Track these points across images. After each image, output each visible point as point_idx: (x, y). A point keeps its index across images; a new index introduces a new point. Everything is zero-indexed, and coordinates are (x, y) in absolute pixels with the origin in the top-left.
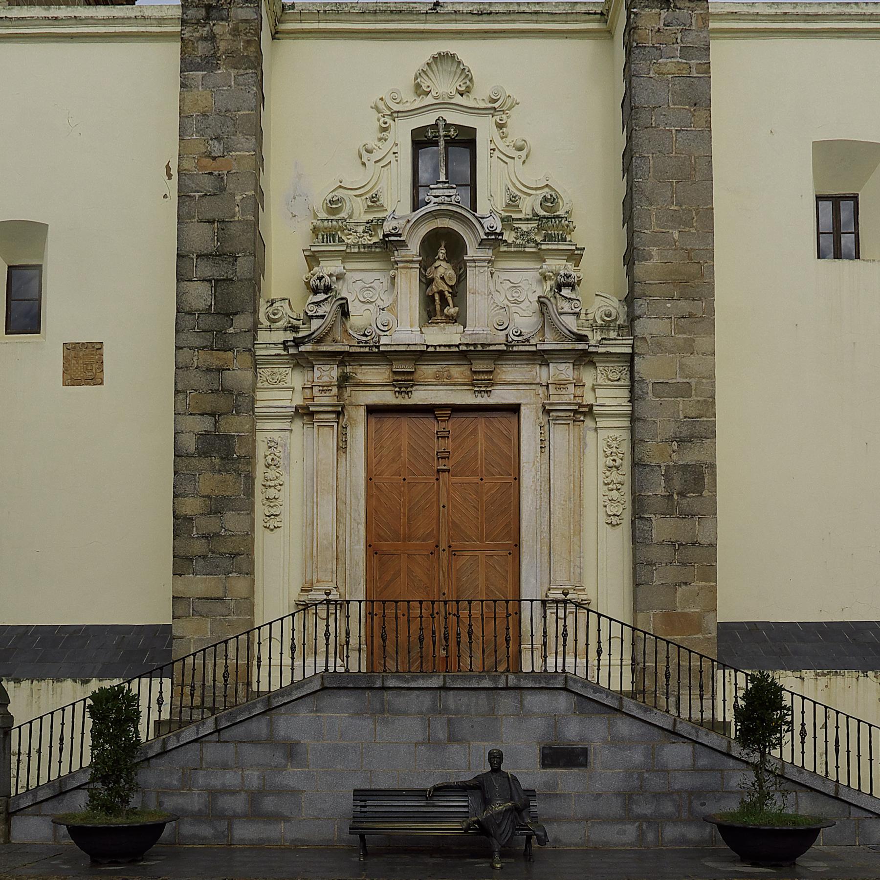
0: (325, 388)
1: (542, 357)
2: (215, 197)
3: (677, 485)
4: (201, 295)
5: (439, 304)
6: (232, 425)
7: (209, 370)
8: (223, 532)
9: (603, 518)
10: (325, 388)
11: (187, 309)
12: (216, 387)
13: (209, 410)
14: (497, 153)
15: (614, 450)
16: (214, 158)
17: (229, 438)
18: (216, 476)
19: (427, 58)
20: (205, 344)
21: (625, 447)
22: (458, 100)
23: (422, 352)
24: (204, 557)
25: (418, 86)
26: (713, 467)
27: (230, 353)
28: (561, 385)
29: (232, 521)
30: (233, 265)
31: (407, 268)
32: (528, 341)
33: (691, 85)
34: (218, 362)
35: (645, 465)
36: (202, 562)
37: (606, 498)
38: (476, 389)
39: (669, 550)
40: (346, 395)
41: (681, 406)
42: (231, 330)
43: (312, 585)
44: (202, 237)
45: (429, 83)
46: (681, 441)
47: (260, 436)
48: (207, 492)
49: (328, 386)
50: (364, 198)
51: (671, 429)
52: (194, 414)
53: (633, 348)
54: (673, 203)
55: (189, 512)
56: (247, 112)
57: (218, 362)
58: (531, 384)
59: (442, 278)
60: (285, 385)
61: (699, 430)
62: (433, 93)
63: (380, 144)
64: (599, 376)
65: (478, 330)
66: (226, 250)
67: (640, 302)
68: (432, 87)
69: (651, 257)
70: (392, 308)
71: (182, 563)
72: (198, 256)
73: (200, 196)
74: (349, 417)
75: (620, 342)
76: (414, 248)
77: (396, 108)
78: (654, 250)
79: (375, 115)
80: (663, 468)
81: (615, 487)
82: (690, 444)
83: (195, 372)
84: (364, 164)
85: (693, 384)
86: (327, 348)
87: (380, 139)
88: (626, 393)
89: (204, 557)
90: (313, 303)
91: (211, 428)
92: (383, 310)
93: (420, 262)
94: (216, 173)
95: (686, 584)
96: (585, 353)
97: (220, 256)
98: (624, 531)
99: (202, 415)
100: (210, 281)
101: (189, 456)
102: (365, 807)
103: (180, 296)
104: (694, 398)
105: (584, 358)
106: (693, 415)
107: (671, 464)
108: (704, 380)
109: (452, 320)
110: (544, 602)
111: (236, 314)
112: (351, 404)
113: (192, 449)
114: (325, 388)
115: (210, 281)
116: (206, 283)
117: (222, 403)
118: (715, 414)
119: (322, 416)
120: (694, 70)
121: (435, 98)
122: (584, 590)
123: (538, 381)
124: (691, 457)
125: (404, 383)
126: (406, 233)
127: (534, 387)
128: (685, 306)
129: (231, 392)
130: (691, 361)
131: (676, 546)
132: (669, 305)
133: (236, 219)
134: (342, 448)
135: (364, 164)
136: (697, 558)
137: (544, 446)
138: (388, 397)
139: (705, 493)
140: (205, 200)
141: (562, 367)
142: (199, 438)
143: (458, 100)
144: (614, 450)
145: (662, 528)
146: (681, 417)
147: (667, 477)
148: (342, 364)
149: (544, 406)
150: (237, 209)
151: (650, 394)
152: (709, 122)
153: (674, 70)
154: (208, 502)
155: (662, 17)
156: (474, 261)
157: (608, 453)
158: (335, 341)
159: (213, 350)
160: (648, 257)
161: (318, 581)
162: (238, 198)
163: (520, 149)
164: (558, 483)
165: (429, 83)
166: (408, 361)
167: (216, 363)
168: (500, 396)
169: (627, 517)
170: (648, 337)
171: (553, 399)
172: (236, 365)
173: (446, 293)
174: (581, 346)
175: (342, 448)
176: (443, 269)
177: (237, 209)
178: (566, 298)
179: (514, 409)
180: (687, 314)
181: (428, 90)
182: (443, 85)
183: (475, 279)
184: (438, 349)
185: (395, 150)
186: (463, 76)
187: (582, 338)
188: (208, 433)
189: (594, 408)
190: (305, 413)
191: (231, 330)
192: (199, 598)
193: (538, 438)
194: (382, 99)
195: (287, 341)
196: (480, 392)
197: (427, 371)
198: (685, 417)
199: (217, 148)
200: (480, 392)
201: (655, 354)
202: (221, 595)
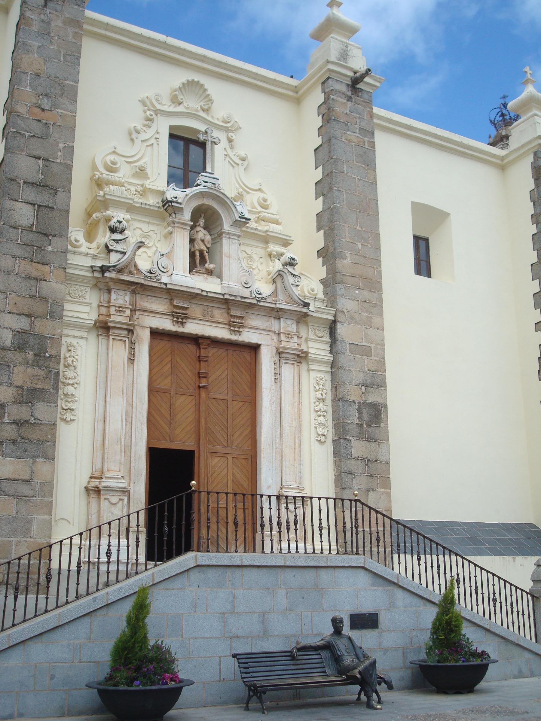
0: (121, 309)
1: (277, 313)
2: (42, 140)
5: (198, 261)
6: (43, 327)
7: (28, 278)
8: (32, 420)
9: (314, 436)
10: (120, 309)
11: (12, 223)
12: (33, 293)
13: (26, 311)
15: (321, 387)
16: (43, 110)
17: (42, 337)
18: (30, 370)
19: (184, 80)
20: (26, 256)
21: (328, 386)
22: (202, 114)
23: (197, 294)
24: (14, 442)
25: (176, 97)
26: (386, 406)
27: (47, 267)
28: (289, 335)
29: (41, 411)
30: (54, 196)
31: (182, 228)
32: (265, 299)
33: (365, 153)
34: (36, 273)
35: (347, 401)
36: (11, 446)
37: (316, 421)
38: (232, 328)
39: (361, 464)
40: (135, 317)
41: (366, 362)
42: (50, 248)
43: (102, 473)
45: (182, 97)
47: (64, 339)
48: (20, 383)
49: (123, 308)
50: (133, 165)
51: (359, 377)
52: (12, 313)
53: (335, 317)
54: (357, 225)
56: (72, 83)
57: (36, 273)
58: (269, 331)
59: (203, 241)
60: (84, 301)
61: (376, 381)
62: (185, 104)
63: (145, 128)
64: (310, 332)
65: (232, 284)
66: (48, 183)
67: (340, 286)
68: (184, 100)
70: (169, 255)
72: (25, 183)
73: (29, 136)
74: (137, 336)
75: (328, 311)
76: (187, 216)
77: (159, 107)
78: (348, 254)
79: (141, 108)
80: (357, 404)
81: (322, 414)
82: (372, 389)
83: (14, 278)
84: (132, 140)
85: (372, 348)
87: (145, 126)
88: (328, 347)
89: (14, 442)
90: (114, 240)
91: (27, 328)
92: (162, 255)
94: (44, 121)
96: (306, 315)
97: (43, 186)
100: (34, 205)
102: (248, 668)
104: (373, 358)
105: (302, 318)
106: (373, 369)
107: (362, 402)
108: (378, 346)
109: (210, 272)
110: (278, 498)
111: (54, 236)
114: (121, 309)
115: (34, 205)
116: (30, 205)
117: (38, 308)
118: (385, 371)
119: (116, 331)
120: (366, 144)
121: (187, 108)
122: (303, 490)
123: (273, 330)
124: (372, 398)
125: (180, 317)
126: (185, 203)
127: (270, 333)
128: (366, 294)
129: (46, 300)
130: (372, 332)
131: (367, 462)
132: (357, 292)
133: (59, 161)
135: (132, 140)
136: (377, 471)
137: (277, 378)
138: (167, 324)
139: (382, 425)
140: (33, 140)
141: (289, 322)
142: (15, 335)
143: (202, 114)
144: (321, 387)
145: (358, 448)
146: (366, 369)
147: (360, 413)
148: (133, 292)
149: (277, 349)
150: (59, 154)
151: (348, 351)
152: (375, 178)
153: (356, 141)
154: (20, 392)
157: (317, 388)
158: (131, 273)
159: (32, 261)
160: (345, 258)
161: (108, 470)
163: (243, 159)
164: (287, 408)
165: (182, 97)
166: (181, 301)
167: (35, 274)
168: (248, 336)
169: (331, 436)
170: (346, 311)
171: (283, 344)
172: (52, 278)
173: (205, 252)
174: (305, 310)
176: (202, 234)
177: (59, 154)
178: (292, 274)
179: (255, 348)
181: (182, 101)
182: (192, 103)
184: (209, 294)
185: (157, 136)
186: (206, 100)
187: (307, 305)
188: (23, 332)
189: (310, 355)
192: (6, 479)
193: (273, 371)
195: (95, 266)
196: (234, 331)
197: (195, 310)
198: (369, 370)
199: (46, 103)
200: (234, 331)
202: (27, 477)
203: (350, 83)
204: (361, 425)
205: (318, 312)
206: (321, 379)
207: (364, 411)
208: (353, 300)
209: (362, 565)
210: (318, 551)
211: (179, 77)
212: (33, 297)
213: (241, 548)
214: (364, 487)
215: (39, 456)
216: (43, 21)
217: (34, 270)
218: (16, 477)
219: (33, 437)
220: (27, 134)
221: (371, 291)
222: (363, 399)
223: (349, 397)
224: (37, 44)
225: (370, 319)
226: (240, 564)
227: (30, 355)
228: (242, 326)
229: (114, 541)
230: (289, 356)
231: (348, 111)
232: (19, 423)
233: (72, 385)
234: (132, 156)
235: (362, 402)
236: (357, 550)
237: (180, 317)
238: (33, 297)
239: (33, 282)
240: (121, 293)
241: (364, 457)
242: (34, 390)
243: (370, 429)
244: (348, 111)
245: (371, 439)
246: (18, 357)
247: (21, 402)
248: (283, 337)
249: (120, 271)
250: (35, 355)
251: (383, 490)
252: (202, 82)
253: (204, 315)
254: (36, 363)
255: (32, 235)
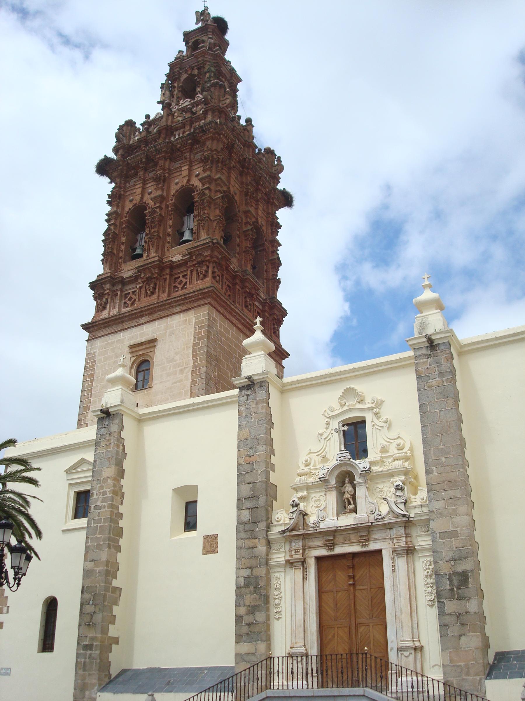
3: (456, 582)
4: (246, 515)
5: (347, 504)
7: (249, 548)
8: (255, 622)
13: (249, 566)
14: (376, 426)
16: (250, 457)
17: (257, 578)
24: (247, 634)
27: (257, 540)
29: (260, 617)
36: (246, 637)
39: (454, 618)
42: (257, 529)
44: (247, 491)
46: (455, 560)
48: (248, 604)
55: (241, 614)
66: (255, 495)
69: (433, 471)
71: (239, 638)
85: (459, 531)
86: (300, 532)
89: (247, 634)
93: (336, 487)
95: (464, 635)
98: (435, 608)
99: (246, 568)
101: (241, 588)
103: (238, 516)
106: (460, 546)
107: (452, 572)
112: (309, 557)
113: (242, 584)
119: (296, 564)
120: (445, 382)
124: (461, 567)
125: (330, 545)
129: (257, 557)
131: (459, 615)
132: (443, 494)
134: (305, 578)
138: (323, 552)
140: (247, 475)
141: (399, 529)
145: (451, 606)
146: (454, 548)
147: (451, 580)
151: (439, 539)
154: (249, 608)
155: (429, 361)
156: (359, 483)
162: (259, 472)
167: (251, 545)
168: (373, 546)
170: (435, 510)
175: (305, 578)
176: (348, 488)
179: (379, 552)
180: (452, 497)
182: (351, 402)
183: (360, 492)
184: (342, 528)
188: (249, 577)
190: (290, 563)
191: (257, 529)
194: (326, 411)
199: (251, 453)
201: (439, 518)
202: (254, 652)
203: (428, 345)
204: (452, 590)
205: (417, 516)
206: (428, 562)
207: (454, 579)
208: (441, 501)
209: (363, 694)
210: (281, 688)
211: (338, 391)
212: (251, 558)
213: (330, 684)
214: (456, 634)
215: (258, 641)
216: (247, 409)
217: (250, 543)
218: (249, 652)
219: (256, 631)
220: (244, 473)
221: (455, 489)
222: (453, 570)
223: (441, 571)
224: (245, 422)
225: (455, 510)
226: (288, 695)
227: (252, 588)
228: (368, 540)
229: (300, 682)
230: (400, 552)
231: (428, 366)
232: (249, 625)
233: (278, 598)
234: (320, 450)
235: (452, 572)
236: (366, 684)
237: (330, 545)
238: (251, 558)
239: (251, 550)
240: (297, 541)
241: (456, 612)
242: (255, 606)
243: (460, 591)
244: (428, 366)
245: (460, 598)
246: (247, 590)
247: (249, 614)
248: (395, 541)
249: (293, 530)
250: (254, 588)
251: (473, 634)
252: (352, 386)
253: (345, 540)
254: (255, 592)
255: (249, 525)
